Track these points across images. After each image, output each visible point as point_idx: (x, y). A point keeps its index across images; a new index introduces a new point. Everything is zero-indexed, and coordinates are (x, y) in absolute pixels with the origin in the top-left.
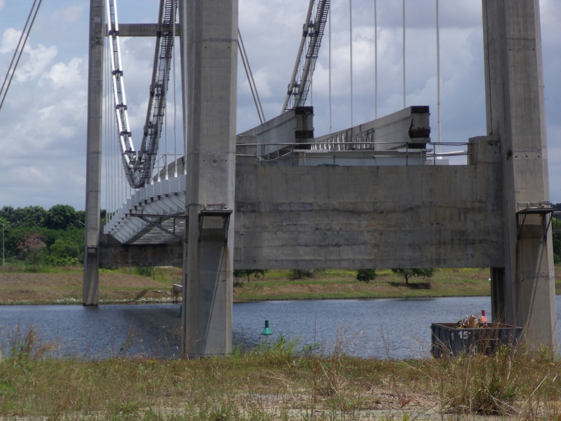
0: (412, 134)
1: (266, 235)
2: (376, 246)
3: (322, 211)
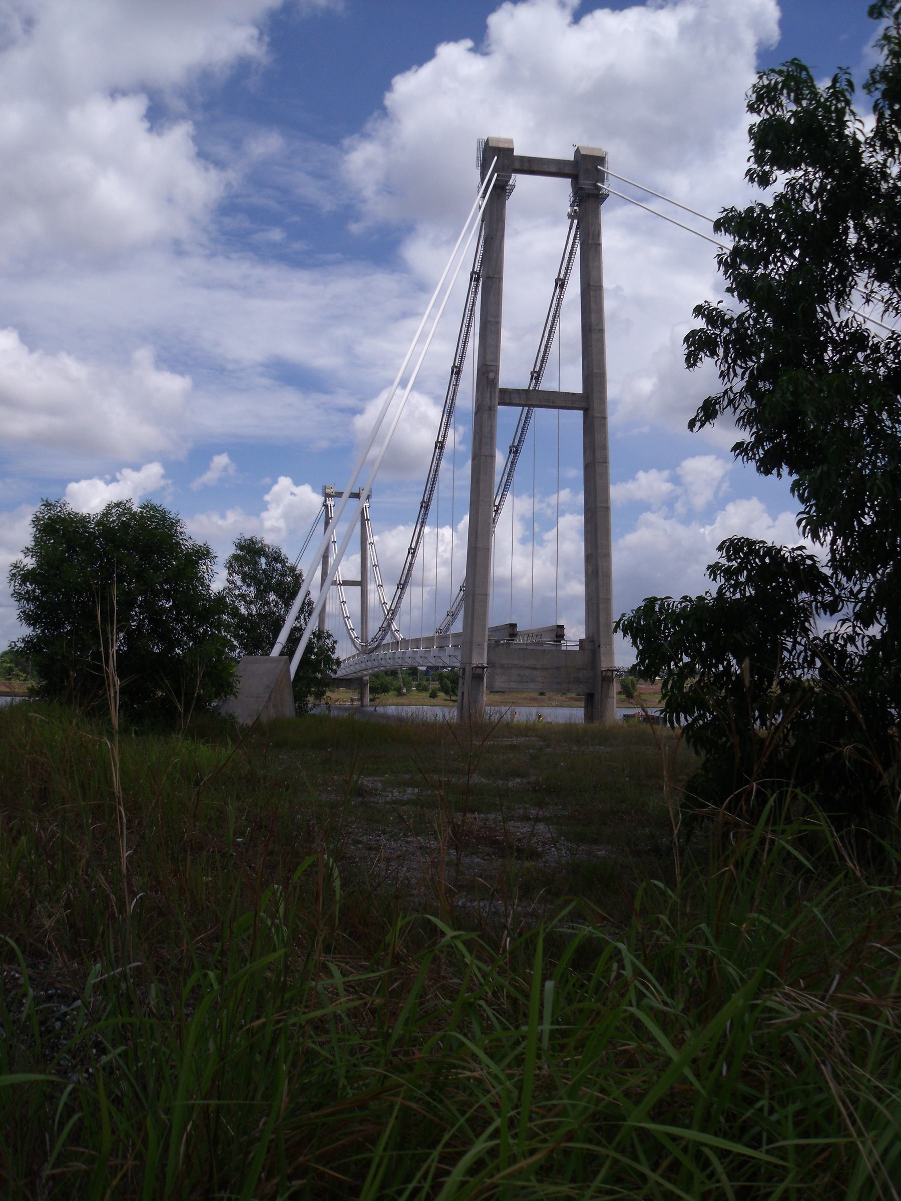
0: (557, 637)
1: (497, 677)
2: (543, 683)
3: (522, 667)
